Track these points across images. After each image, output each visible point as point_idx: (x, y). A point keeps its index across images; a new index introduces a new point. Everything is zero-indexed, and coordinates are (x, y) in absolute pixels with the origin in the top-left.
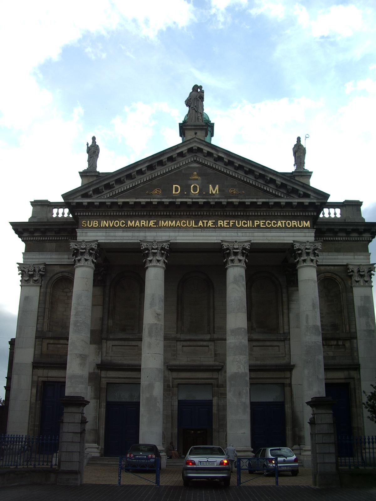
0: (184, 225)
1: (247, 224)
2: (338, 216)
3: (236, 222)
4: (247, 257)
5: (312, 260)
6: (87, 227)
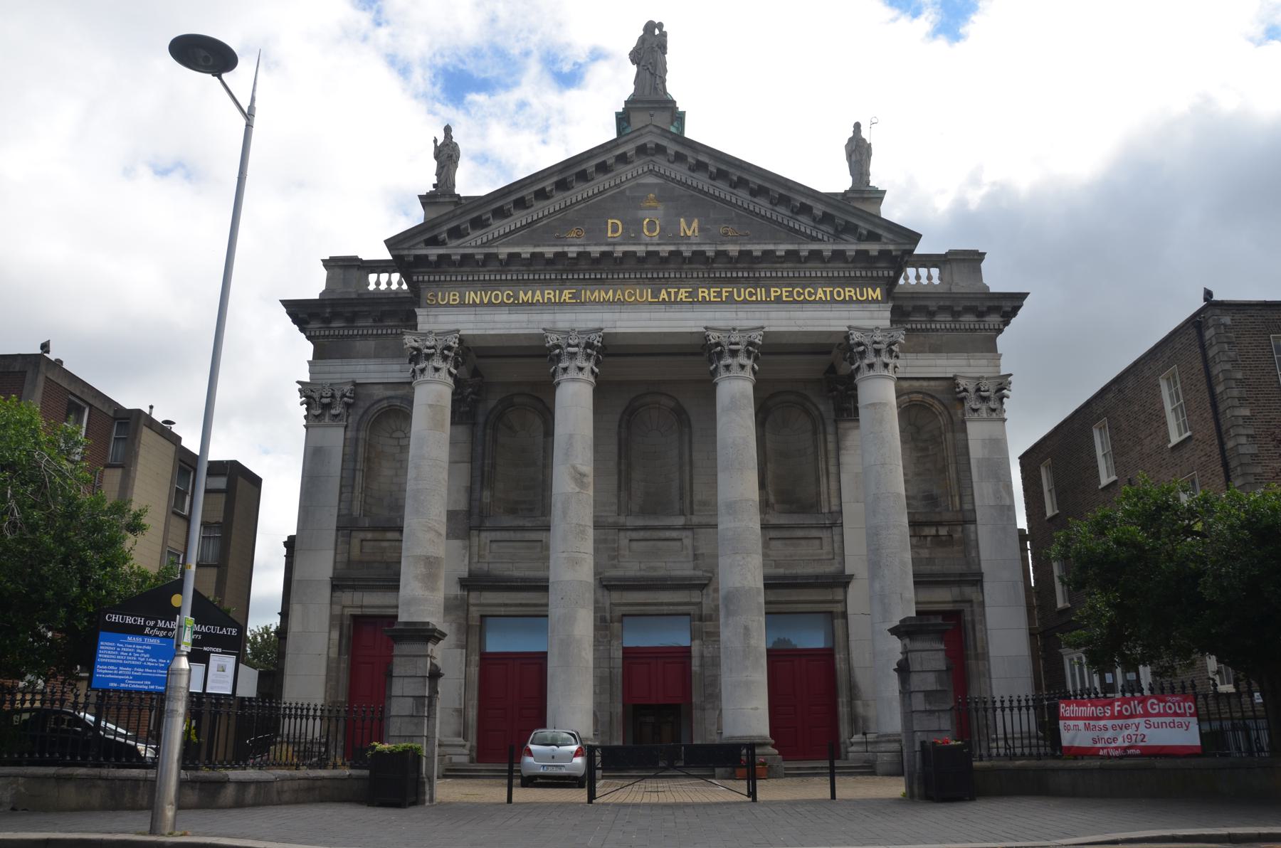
1: (756, 294)
3: (733, 291)
4: (756, 359)
5: (886, 365)
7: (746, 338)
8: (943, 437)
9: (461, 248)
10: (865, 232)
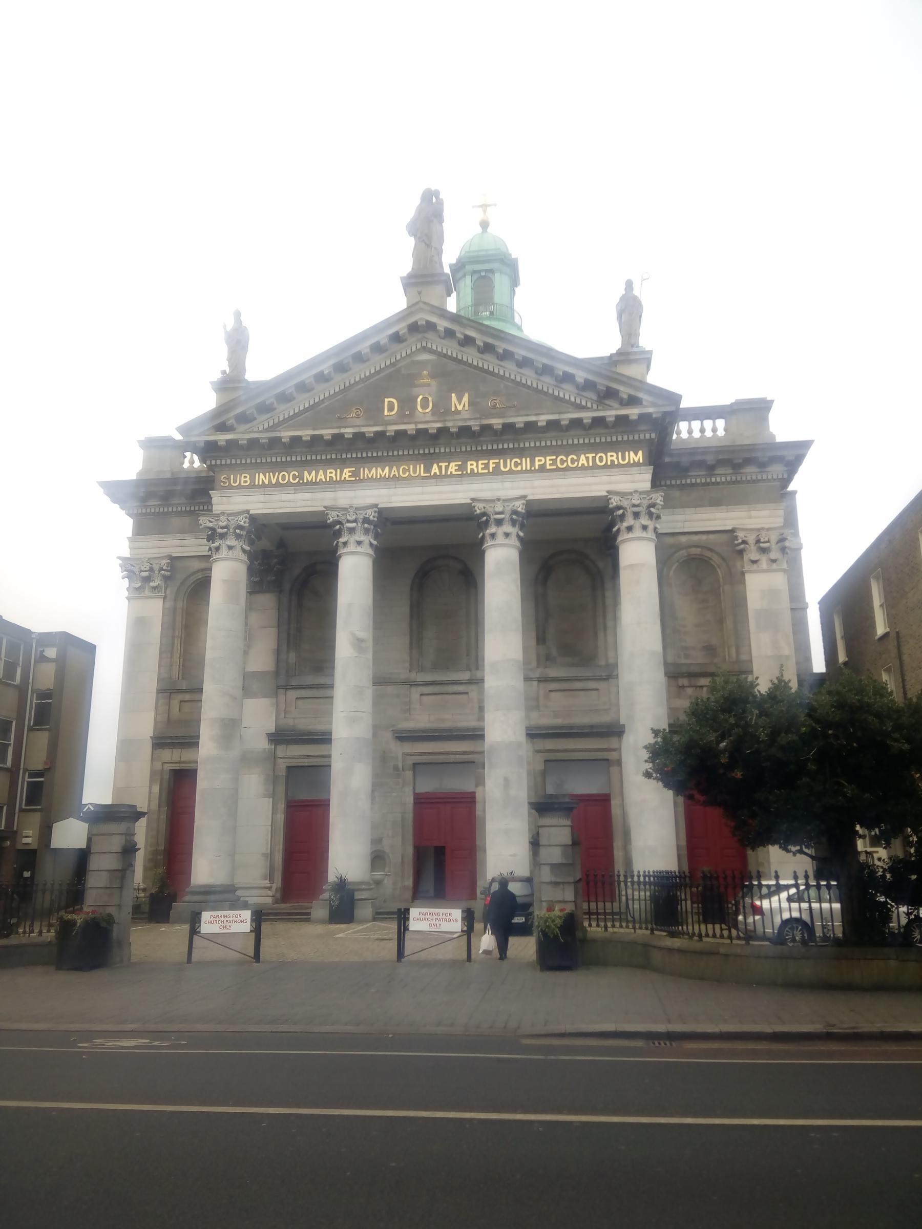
0: (295, 480)
1: (521, 464)
2: (721, 433)
3: (500, 462)
4: (522, 527)
5: (645, 528)
6: (231, 487)
7: (511, 506)
8: (721, 588)
9: (247, 433)
10: (625, 397)
